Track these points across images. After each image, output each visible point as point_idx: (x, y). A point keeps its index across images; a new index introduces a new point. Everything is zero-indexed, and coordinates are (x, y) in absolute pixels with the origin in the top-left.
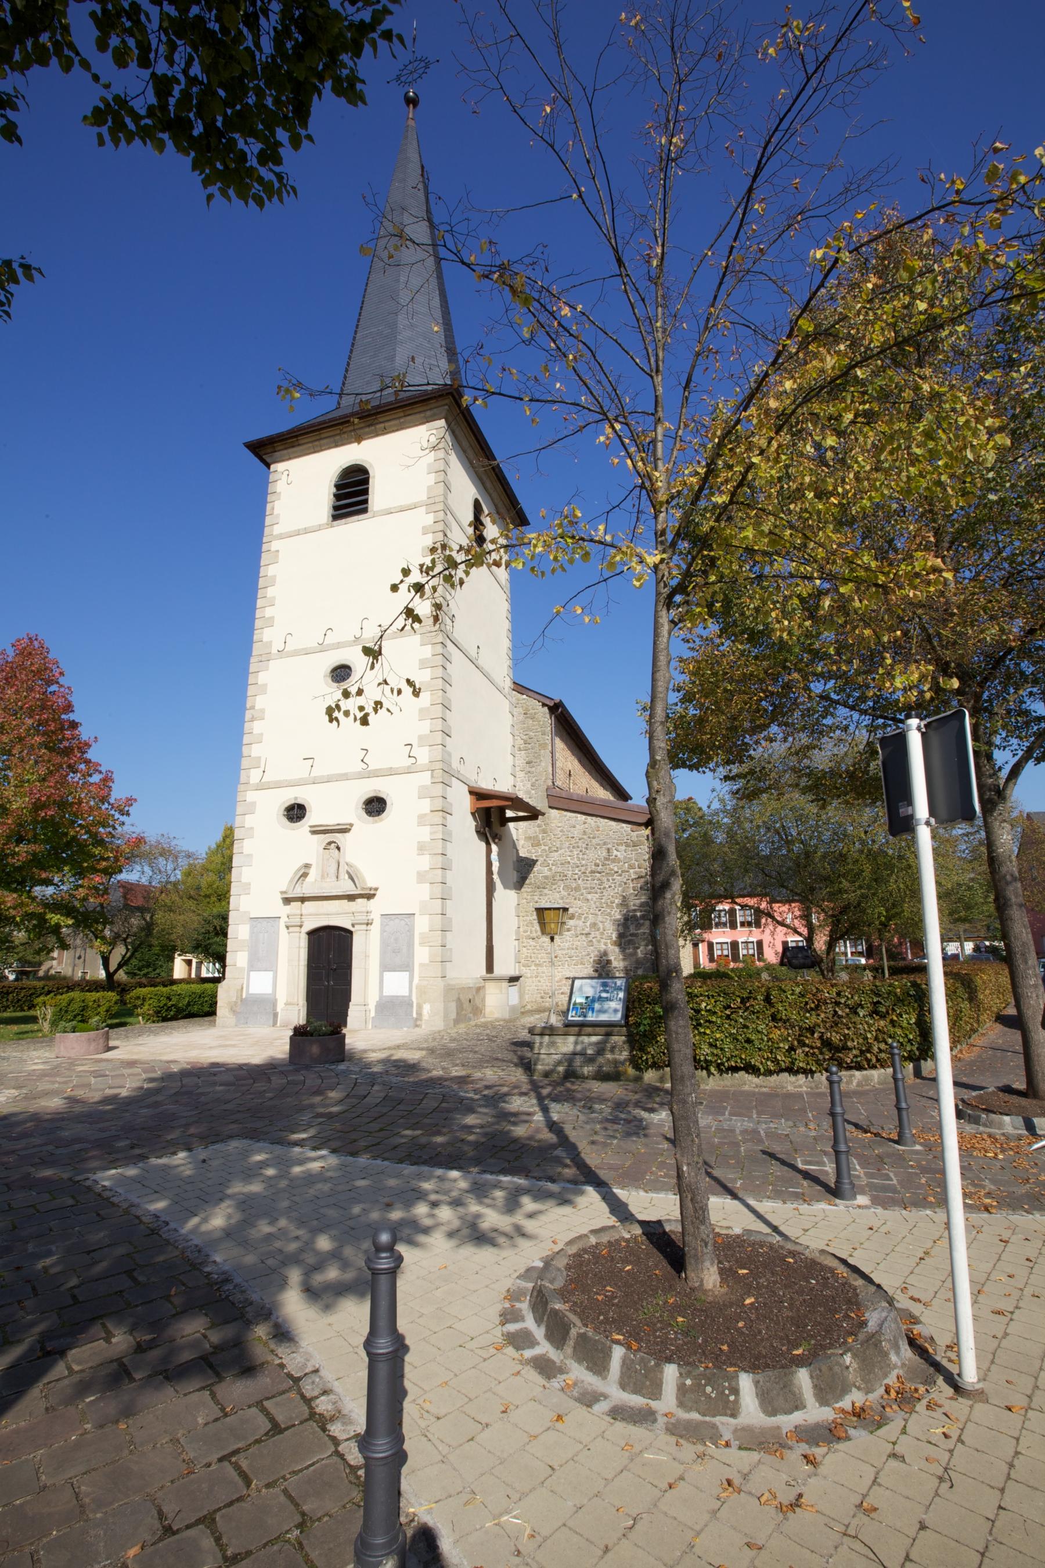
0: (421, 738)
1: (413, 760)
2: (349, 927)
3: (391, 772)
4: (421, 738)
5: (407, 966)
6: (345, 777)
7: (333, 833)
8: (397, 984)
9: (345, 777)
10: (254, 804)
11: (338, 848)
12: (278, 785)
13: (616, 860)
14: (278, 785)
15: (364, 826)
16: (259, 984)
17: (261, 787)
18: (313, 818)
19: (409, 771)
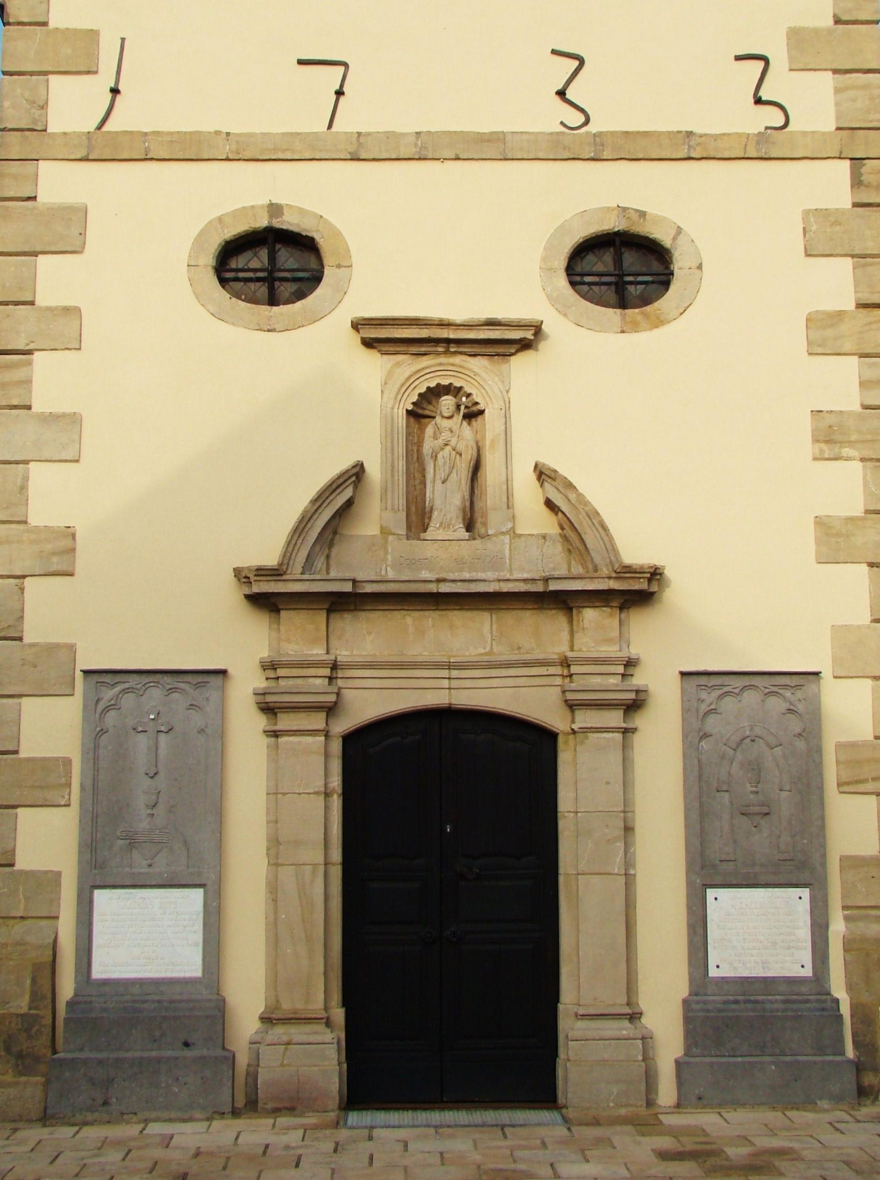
0: (798, 39)
1: (776, 118)
2: (553, 718)
3: (689, 149)
4: (798, 39)
6: (495, 148)
7: (443, 359)
9: (495, 148)
10: (75, 216)
12: (188, 150)
14: (188, 150)
15: (585, 341)
17: (101, 147)
18: (373, 278)
19: (762, 150)
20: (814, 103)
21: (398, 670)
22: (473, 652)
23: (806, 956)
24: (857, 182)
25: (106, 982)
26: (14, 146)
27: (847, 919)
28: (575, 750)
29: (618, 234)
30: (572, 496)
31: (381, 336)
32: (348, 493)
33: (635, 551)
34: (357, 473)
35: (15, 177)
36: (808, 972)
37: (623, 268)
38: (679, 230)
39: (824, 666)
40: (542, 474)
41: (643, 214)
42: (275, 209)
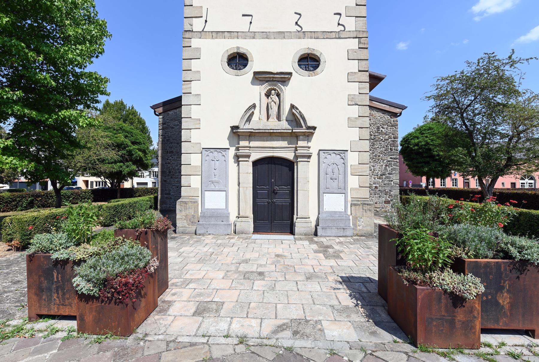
3: (326, 35)
5: (342, 190)
6: (281, 35)
7: (273, 81)
8: (334, 203)
9: (281, 35)
10: (198, 49)
11: (278, 95)
13: (382, 133)
15: (300, 80)
16: (213, 201)
17: (202, 33)
18: (257, 64)
19: (338, 36)
20: (351, 24)
21: (260, 150)
22: (263, 238)
24: (360, 43)
25: (207, 209)
26: (187, 35)
28: (356, 38)
29: (308, 54)
30: (298, 111)
31: (260, 77)
32: (251, 112)
33: (310, 124)
34: (254, 106)
35: (187, 42)
36: (343, 210)
37: (310, 62)
38: (321, 53)
39: (349, 149)
40: (292, 107)
41: (314, 50)
42: (238, 48)
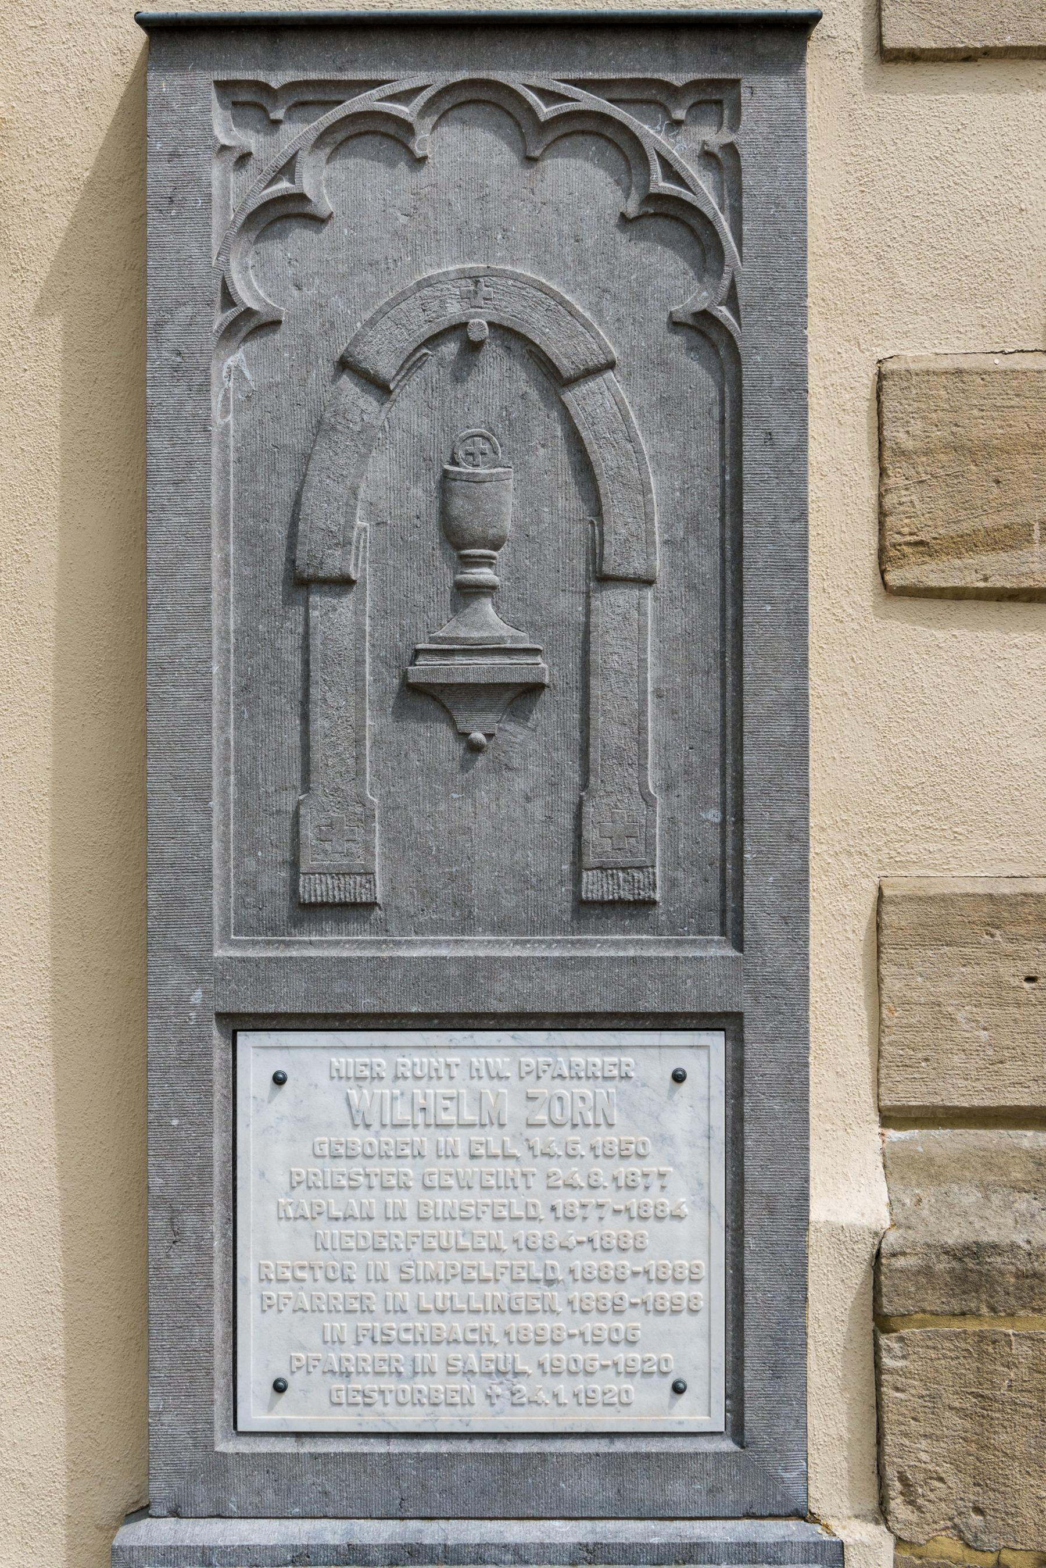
23: (696, 1346)
27: (893, 1165)
36: (703, 1411)
